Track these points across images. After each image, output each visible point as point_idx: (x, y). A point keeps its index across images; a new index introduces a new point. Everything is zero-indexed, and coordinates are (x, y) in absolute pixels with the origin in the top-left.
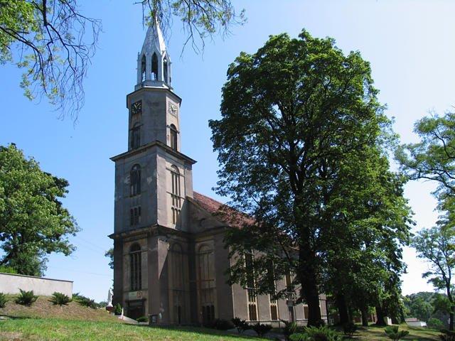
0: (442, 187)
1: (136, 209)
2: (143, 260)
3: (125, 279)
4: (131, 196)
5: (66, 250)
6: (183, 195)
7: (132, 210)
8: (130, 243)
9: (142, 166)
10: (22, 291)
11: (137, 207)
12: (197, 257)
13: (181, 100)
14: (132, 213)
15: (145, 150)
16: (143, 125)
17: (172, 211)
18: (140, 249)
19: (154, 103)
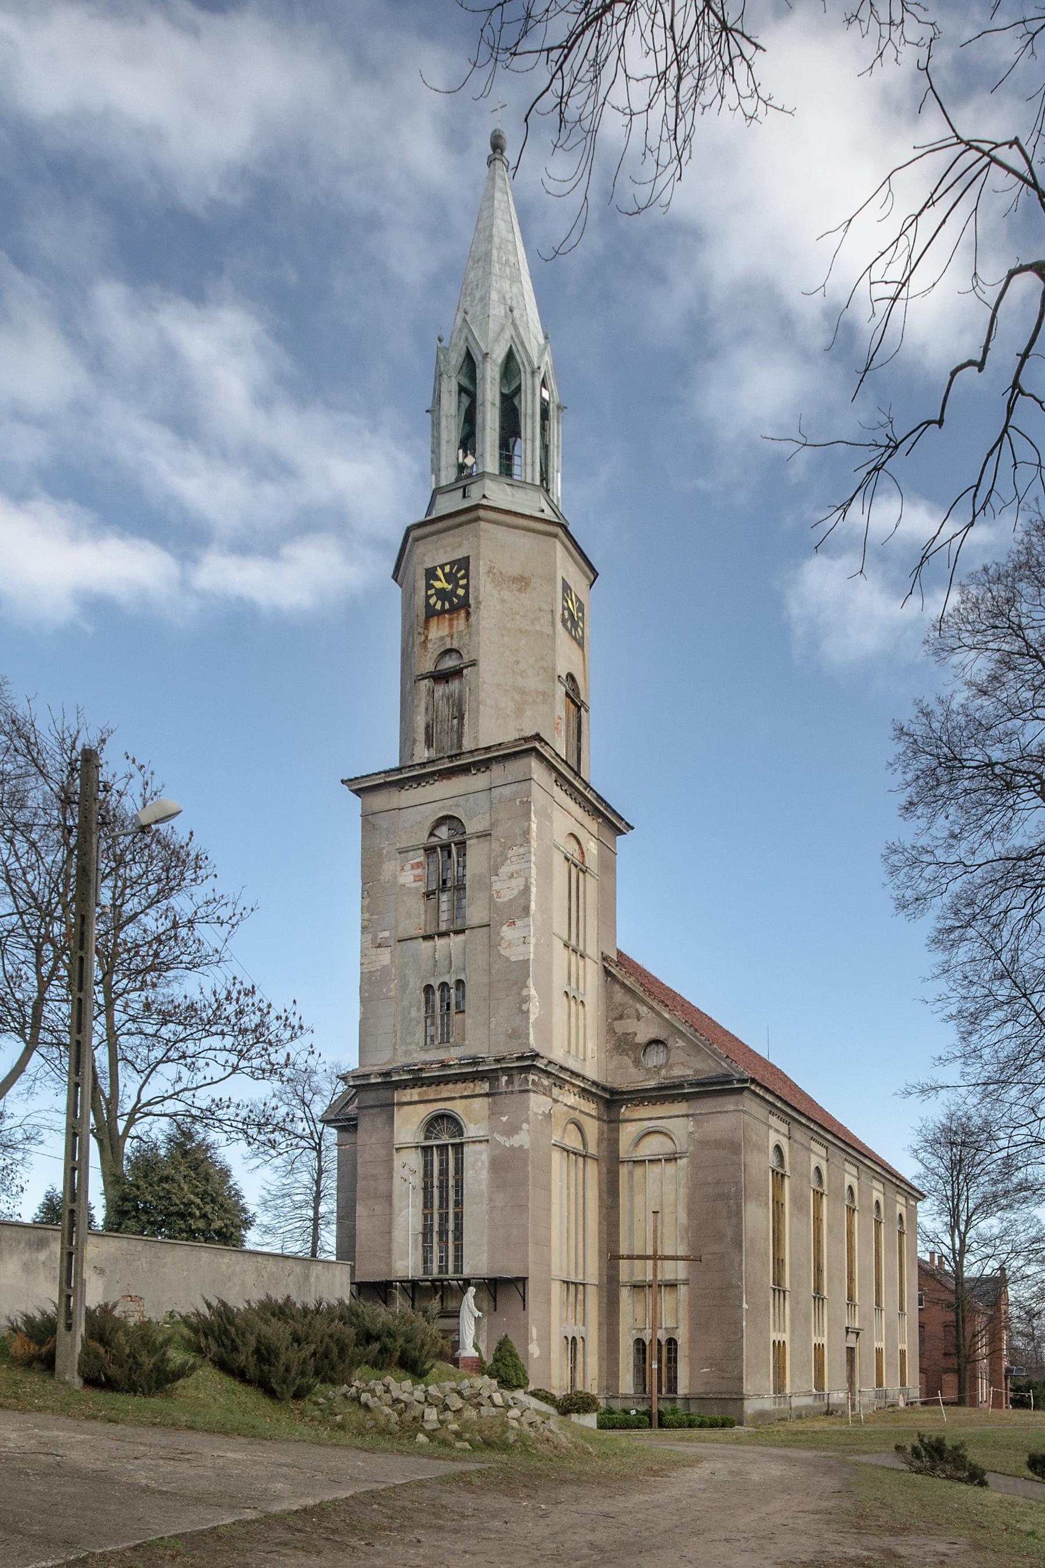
0: (808, 1394)
1: (444, 985)
2: (468, 1174)
3: (398, 1234)
4: (427, 938)
5: (93, 1208)
8: (424, 1111)
9: (472, 827)
10: (343, 1078)
11: (451, 981)
12: (624, 1170)
13: (596, 575)
15: (485, 765)
17: (771, 1291)
18: (461, 1134)
19: (514, 580)
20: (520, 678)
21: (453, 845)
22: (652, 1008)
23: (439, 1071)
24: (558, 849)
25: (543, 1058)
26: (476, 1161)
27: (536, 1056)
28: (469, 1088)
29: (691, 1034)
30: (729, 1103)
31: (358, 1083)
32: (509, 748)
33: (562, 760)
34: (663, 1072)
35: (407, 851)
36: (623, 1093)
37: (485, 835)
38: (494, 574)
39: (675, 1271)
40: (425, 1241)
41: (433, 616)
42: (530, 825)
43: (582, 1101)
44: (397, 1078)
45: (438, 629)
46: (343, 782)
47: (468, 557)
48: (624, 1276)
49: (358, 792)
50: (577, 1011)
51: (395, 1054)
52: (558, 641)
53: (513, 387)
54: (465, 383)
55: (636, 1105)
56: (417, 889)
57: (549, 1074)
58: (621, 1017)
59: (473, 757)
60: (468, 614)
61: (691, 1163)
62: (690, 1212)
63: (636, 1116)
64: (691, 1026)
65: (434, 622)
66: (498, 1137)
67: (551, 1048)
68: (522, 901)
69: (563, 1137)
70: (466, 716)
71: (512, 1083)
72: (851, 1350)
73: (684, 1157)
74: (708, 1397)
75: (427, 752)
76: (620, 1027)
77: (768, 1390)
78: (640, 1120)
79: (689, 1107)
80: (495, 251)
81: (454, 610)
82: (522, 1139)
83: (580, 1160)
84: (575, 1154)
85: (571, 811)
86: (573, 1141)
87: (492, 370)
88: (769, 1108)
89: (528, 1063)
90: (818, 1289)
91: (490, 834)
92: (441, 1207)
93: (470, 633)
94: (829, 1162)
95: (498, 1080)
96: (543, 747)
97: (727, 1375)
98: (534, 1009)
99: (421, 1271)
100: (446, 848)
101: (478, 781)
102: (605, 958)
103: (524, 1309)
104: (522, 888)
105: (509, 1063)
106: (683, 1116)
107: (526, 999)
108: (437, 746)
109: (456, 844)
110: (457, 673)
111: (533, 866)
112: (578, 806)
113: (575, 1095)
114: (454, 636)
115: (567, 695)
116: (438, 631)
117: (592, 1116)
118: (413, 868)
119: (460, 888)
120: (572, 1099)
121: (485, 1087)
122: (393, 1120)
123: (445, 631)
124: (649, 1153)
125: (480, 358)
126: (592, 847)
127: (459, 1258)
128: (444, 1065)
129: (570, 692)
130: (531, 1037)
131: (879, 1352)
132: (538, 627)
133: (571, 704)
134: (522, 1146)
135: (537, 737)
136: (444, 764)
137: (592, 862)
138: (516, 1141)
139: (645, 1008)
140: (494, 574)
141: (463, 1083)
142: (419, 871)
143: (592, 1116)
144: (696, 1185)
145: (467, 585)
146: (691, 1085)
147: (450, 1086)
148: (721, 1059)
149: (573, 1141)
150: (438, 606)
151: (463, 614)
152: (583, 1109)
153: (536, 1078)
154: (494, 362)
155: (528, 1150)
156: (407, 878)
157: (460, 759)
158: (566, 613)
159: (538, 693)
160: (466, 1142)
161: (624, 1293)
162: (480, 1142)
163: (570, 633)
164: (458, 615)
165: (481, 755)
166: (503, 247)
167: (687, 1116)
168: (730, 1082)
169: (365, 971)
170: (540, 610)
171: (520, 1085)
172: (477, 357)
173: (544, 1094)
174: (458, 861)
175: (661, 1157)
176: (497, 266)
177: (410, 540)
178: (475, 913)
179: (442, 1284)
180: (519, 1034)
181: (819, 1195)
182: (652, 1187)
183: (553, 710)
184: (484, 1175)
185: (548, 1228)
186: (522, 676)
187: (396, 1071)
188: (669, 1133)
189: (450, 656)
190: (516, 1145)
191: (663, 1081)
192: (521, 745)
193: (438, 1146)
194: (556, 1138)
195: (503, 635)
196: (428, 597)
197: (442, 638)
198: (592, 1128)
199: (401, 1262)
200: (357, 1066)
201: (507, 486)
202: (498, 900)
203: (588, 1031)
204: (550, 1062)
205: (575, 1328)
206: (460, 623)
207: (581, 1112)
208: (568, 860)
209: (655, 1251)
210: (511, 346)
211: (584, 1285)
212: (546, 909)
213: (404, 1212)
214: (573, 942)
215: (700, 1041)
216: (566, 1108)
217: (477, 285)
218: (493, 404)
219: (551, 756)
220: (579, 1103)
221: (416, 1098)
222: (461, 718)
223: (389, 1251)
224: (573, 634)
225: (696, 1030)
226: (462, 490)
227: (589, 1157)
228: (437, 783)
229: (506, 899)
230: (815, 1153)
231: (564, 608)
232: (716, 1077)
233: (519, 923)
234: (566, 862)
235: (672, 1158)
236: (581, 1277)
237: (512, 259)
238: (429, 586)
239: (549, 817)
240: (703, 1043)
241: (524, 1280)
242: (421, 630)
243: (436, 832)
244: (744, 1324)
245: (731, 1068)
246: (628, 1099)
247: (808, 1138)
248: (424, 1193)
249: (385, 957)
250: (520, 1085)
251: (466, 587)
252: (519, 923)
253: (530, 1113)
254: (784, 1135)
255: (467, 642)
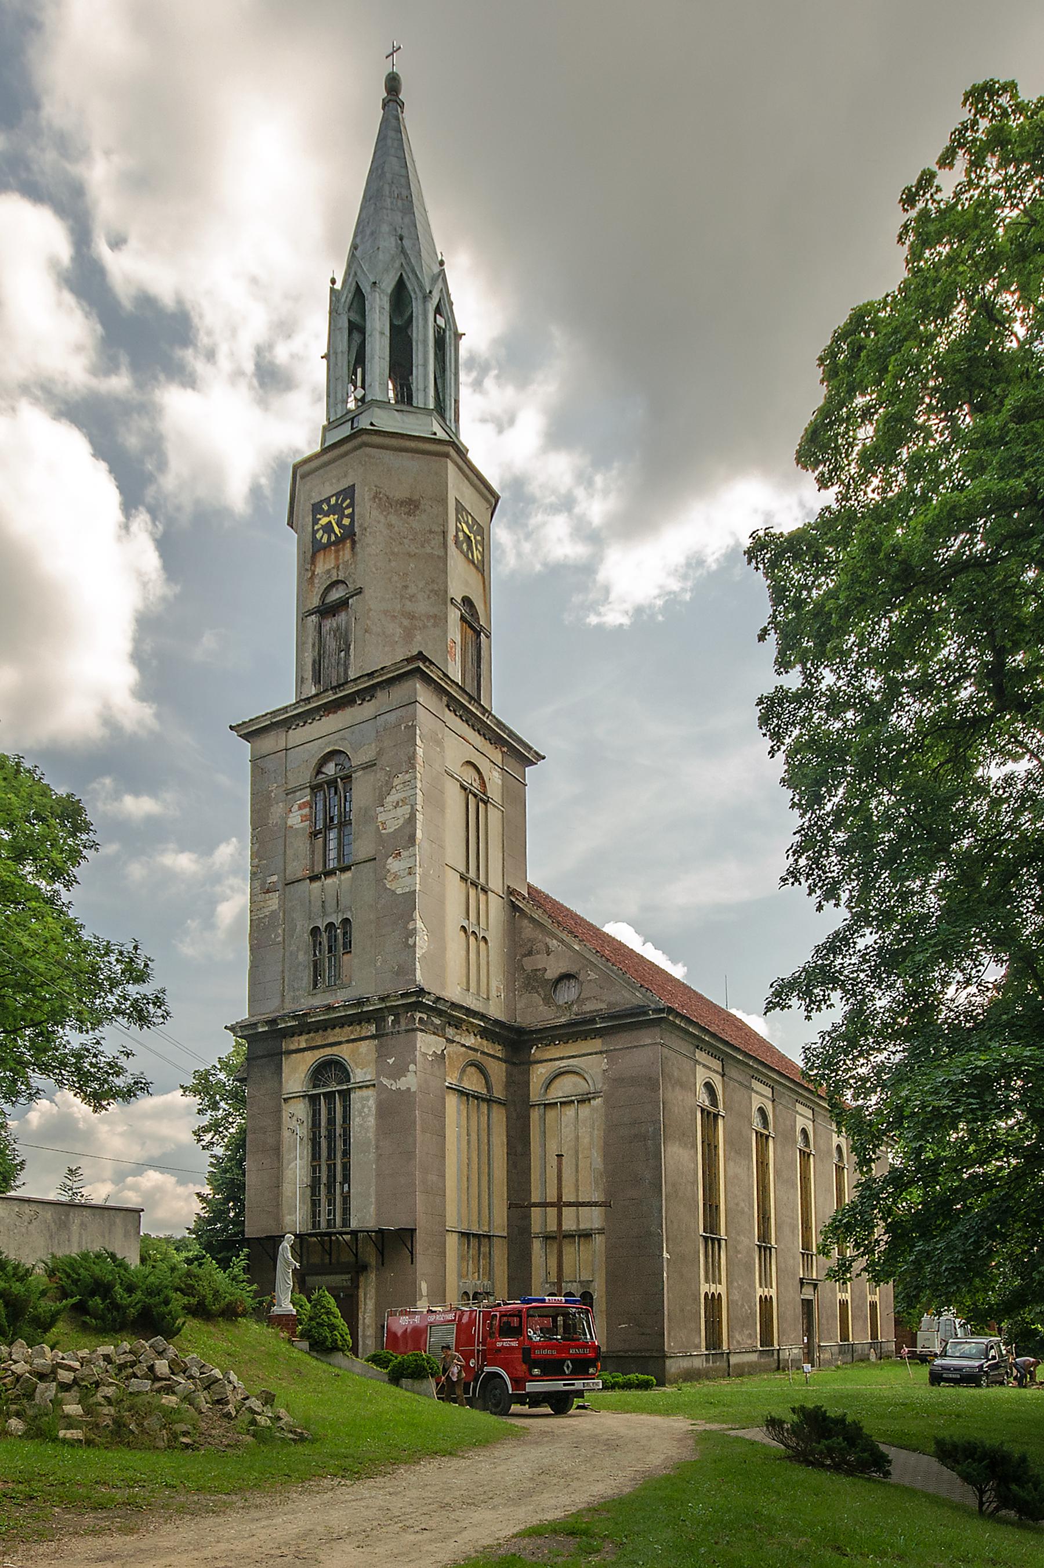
1: (331, 925)
2: (356, 1121)
3: (287, 1189)
4: (314, 878)
6: (495, 883)
7: (315, 931)
8: (311, 1059)
9: (358, 759)
11: (336, 919)
12: (535, 1115)
14: (316, 944)
15: (367, 694)
16: (359, 591)
17: (801, 1256)
19: (402, 503)
20: (408, 603)
21: (339, 780)
22: (562, 941)
23: (324, 1015)
24: (452, 776)
25: (429, 993)
26: (363, 1107)
27: (421, 992)
28: (356, 1031)
29: (602, 964)
30: (646, 1037)
31: (245, 1033)
32: (393, 671)
33: (460, 687)
34: (575, 1008)
35: (294, 792)
36: (532, 1032)
37: (369, 766)
38: (380, 499)
39: (593, 1219)
40: (313, 1194)
41: (319, 551)
42: (415, 749)
43: (485, 1042)
44: (283, 1026)
45: (324, 563)
46: (231, 727)
47: (354, 485)
48: (536, 1227)
49: (247, 737)
50: (478, 947)
51: (283, 1001)
52: (451, 562)
53: (406, 317)
54: (355, 318)
55: (547, 1045)
56: (303, 829)
57: (440, 1013)
58: (530, 953)
59: (357, 685)
60: (354, 543)
61: (606, 1102)
62: (606, 1156)
63: (548, 1056)
64: (603, 956)
65: (320, 557)
66: (385, 1081)
67: (443, 987)
68: (408, 830)
69: (461, 1080)
70: (352, 647)
71: (399, 1023)
72: (807, 1304)
73: (598, 1097)
74: (627, 1355)
75: (314, 688)
76: (528, 963)
77: (698, 1347)
78: (551, 1060)
79: (603, 1044)
80: (387, 187)
81: (340, 541)
82: (409, 1082)
83: (484, 1107)
84: (477, 1098)
85: (467, 738)
86: (473, 1083)
87: (381, 299)
88: (696, 1043)
89: (413, 999)
90: (764, 1236)
91: (375, 764)
92: (329, 1158)
93: (355, 562)
94: (775, 1103)
95: (384, 1021)
96: (427, 667)
97: (648, 1331)
98: (422, 943)
99: (310, 1227)
100: (332, 783)
101: (365, 710)
102: (511, 892)
103: (412, 1263)
104: (407, 816)
105: (394, 1001)
106: (596, 1053)
107: (413, 933)
108: (324, 682)
109: (342, 780)
110: (343, 604)
111: (418, 791)
112: (477, 733)
113: (475, 1035)
114: (340, 567)
115: (463, 618)
116: (324, 565)
117: (498, 1058)
118: (300, 808)
119: (345, 823)
120: (471, 1041)
121: (373, 1029)
122: (281, 1069)
123: (331, 563)
124: (561, 1095)
125: (368, 289)
126: (494, 779)
127: (346, 1211)
128: (329, 1008)
129: (469, 618)
130: (418, 972)
131: (843, 1304)
132: (428, 550)
133: (469, 630)
134: (409, 1089)
135: (421, 656)
136: (329, 697)
137: (494, 791)
138: (403, 1084)
139: (555, 941)
140: (380, 499)
141: (349, 1026)
142: (306, 811)
143: (498, 1058)
144: (611, 1128)
145: (353, 514)
146: (603, 1019)
147: (337, 1030)
148: (635, 989)
149: (473, 1083)
150: (325, 540)
151: (348, 544)
152: (486, 1050)
153: (425, 1016)
154: (383, 291)
155: (415, 1092)
156: (295, 819)
157: (344, 690)
158: (461, 534)
159: (429, 617)
160: (352, 1088)
161: (537, 1245)
162: (367, 1087)
163: (467, 557)
164: (344, 545)
165: (365, 682)
166: (395, 181)
167: (601, 1052)
168: (646, 1013)
169: (254, 918)
170: (431, 532)
171: (407, 1025)
172: (366, 289)
173: (434, 1033)
174: (345, 797)
175: (573, 1098)
176: (389, 200)
177: (298, 478)
178: (361, 847)
179: (331, 1239)
180: (406, 970)
181: (763, 1139)
182: (567, 1132)
183: (445, 633)
184: (372, 1121)
185: (442, 1176)
186: (411, 601)
187: (283, 1018)
188: (582, 1072)
189: (337, 589)
190: (403, 1088)
191: (575, 1017)
192: (403, 667)
193: (324, 1094)
194: (451, 1080)
195: (390, 560)
196: (314, 532)
197: (328, 571)
198: (497, 1070)
199: (289, 1217)
200: (247, 1017)
201: (396, 412)
202: (383, 831)
203: (491, 969)
204: (438, 999)
205: (478, 1282)
206: (346, 554)
207: (483, 1053)
208: (465, 789)
209: (560, 1197)
210: (401, 274)
211: (489, 1237)
212: (437, 841)
213: (292, 1165)
214: (472, 874)
215: (612, 971)
216: (464, 1049)
217: (368, 223)
218: (382, 333)
219: (439, 677)
220: (481, 1044)
221: (303, 1045)
222: (347, 650)
223: (278, 1206)
224: (470, 556)
225: (608, 960)
226: (350, 422)
227: (495, 1102)
228: (323, 718)
229: (392, 830)
230: (757, 1093)
231: (457, 530)
232: (632, 1008)
233: (404, 854)
234: (463, 791)
235: (584, 1099)
236: (486, 1229)
237: (405, 193)
238: (315, 521)
239: (439, 743)
240: (615, 973)
241: (413, 1231)
242: (308, 567)
243: (324, 770)
244: (665, 1275)
245: (648, 998)
246: (539, 1038)
247: (748, 1077)
248: (312, 1143)
249: (273, 902)
250: (407, 1025)
251: (351, 516)
252: (404, 854)
253: (418, 1053)
254: (717, 1072)
255: (353, 571)
